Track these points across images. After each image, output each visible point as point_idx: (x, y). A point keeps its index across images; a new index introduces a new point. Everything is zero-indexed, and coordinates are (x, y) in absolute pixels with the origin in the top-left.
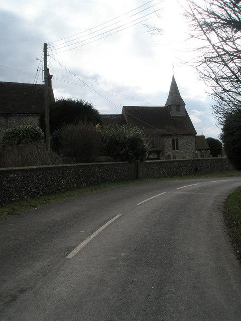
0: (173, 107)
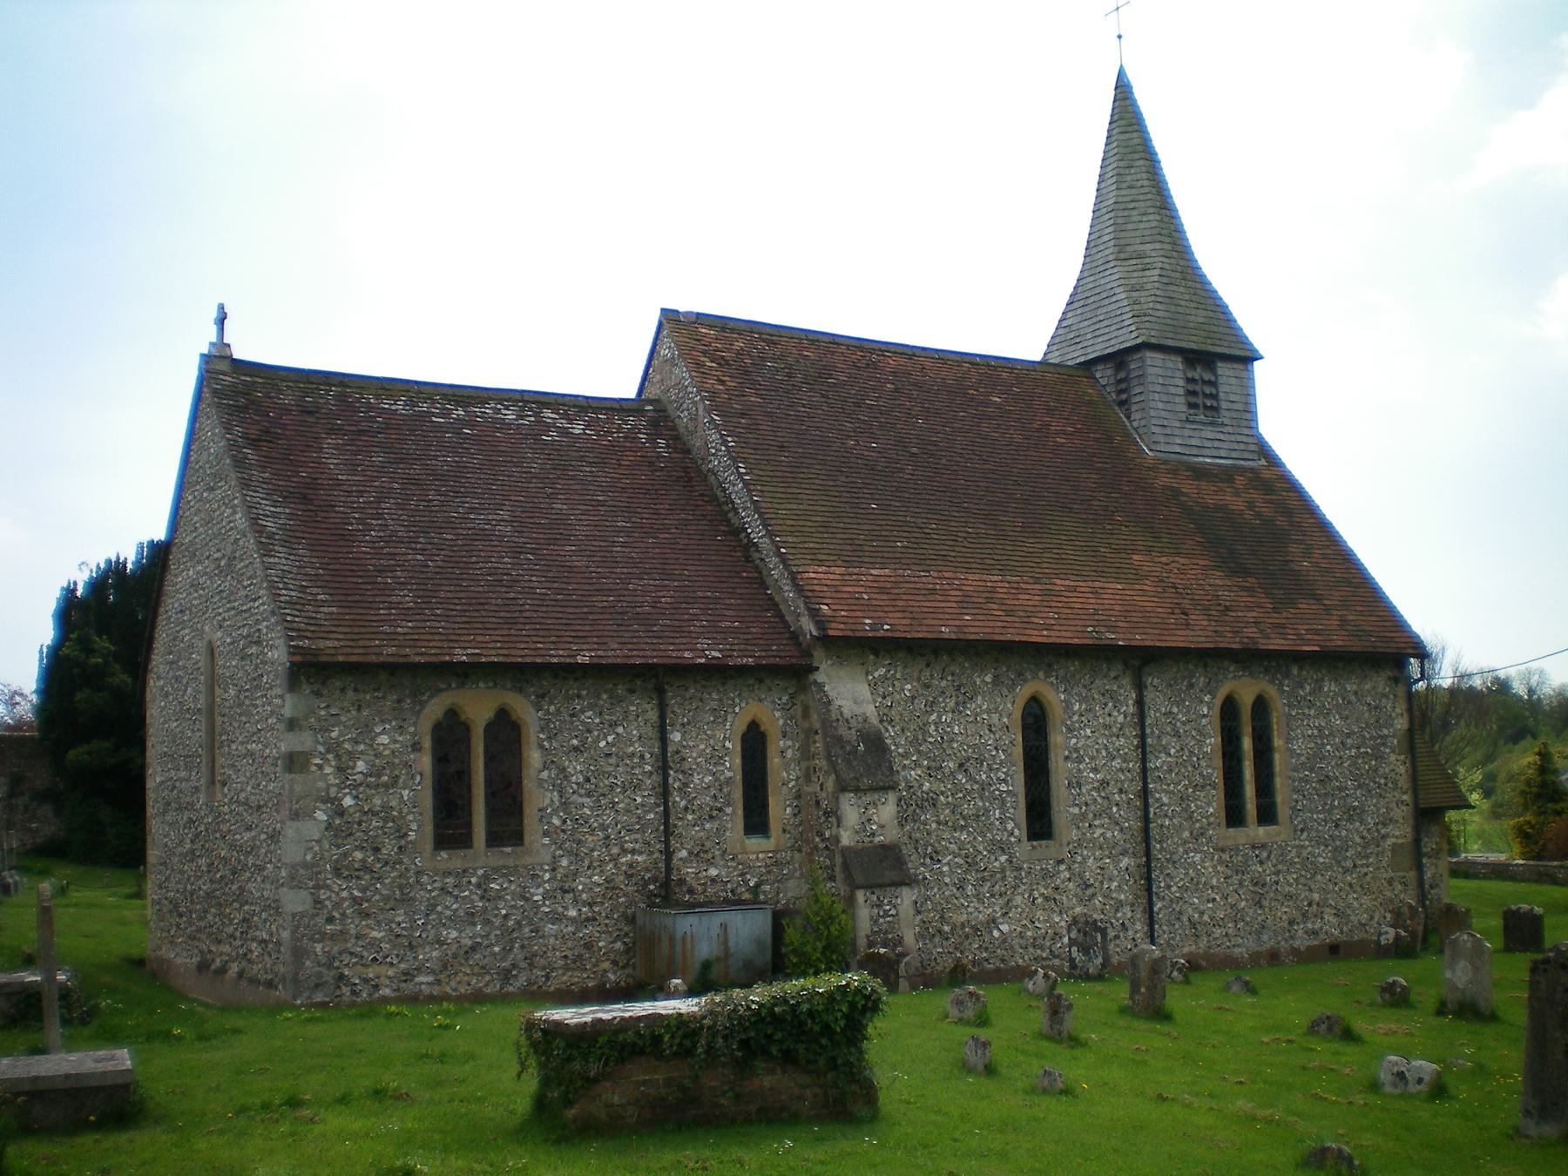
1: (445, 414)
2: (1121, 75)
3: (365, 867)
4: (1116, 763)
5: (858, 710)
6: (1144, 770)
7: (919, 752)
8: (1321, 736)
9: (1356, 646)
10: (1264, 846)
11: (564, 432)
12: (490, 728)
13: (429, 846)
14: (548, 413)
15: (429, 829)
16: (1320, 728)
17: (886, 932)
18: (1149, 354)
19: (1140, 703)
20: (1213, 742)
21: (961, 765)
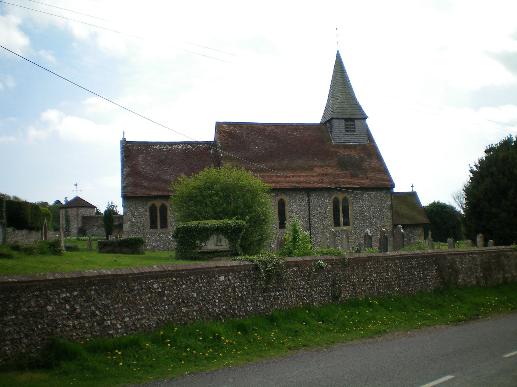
0: (335, 122)
1: (167, 148)
2: (338, 52)
3: (137, 232)
4: (303, 213)
9: (375, 185)
11: (191, 150)
12: (160, 207)
13: (149, 228)
14: (189, 146)
15: (149, 225)
16: (363, 205)
18: (334, 120)
19: (309, 200)
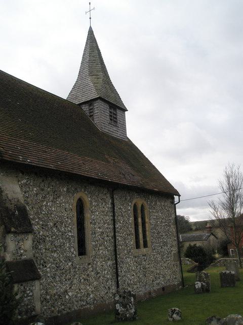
4: (106, 225)
5: (15, 196)
6: (114, 228)
7: (39, 218)
8: (157, 219)
10: (145, 255)
17: (28, 305)
19: (113, 204)
20: (132, 219)
21: (55, 224)
